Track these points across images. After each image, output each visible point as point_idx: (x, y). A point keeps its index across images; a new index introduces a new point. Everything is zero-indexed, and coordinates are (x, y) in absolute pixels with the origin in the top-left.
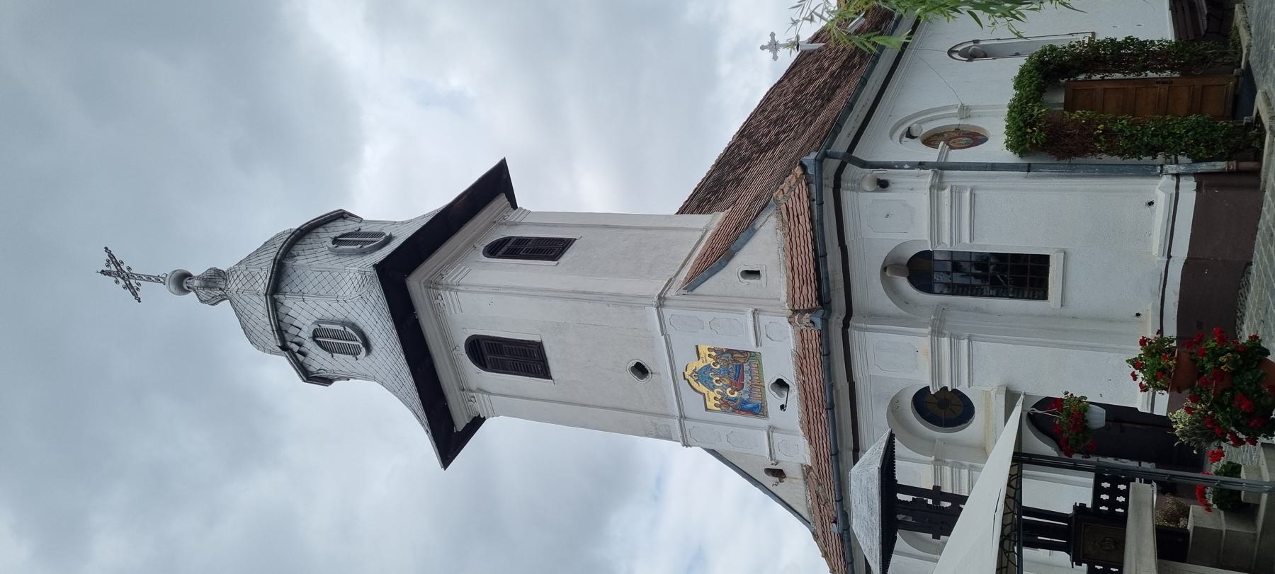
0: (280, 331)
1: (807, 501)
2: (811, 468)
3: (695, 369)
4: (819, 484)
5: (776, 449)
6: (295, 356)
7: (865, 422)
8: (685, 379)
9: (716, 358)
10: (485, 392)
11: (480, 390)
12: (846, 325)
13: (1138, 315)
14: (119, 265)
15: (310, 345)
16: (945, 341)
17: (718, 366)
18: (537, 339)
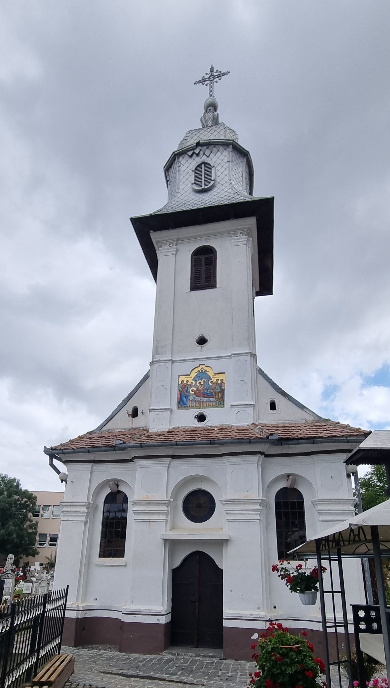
0: (209, 144)
1: (117, 429)
2: (148, 432)
3: (207, 371)
4: (141, 436)
5: (159, 413)
6: (191, 150)
7: (163, 462)
8: (200, 365)
9: (216, 383)
10: (176, 253)
11: (177, 251)
12: (262, 453)
13: (275, 607)
14: (218, 77)
15: (196, 161)
16: (258, 507)
17: (211, 384)
18: (218, 285)
